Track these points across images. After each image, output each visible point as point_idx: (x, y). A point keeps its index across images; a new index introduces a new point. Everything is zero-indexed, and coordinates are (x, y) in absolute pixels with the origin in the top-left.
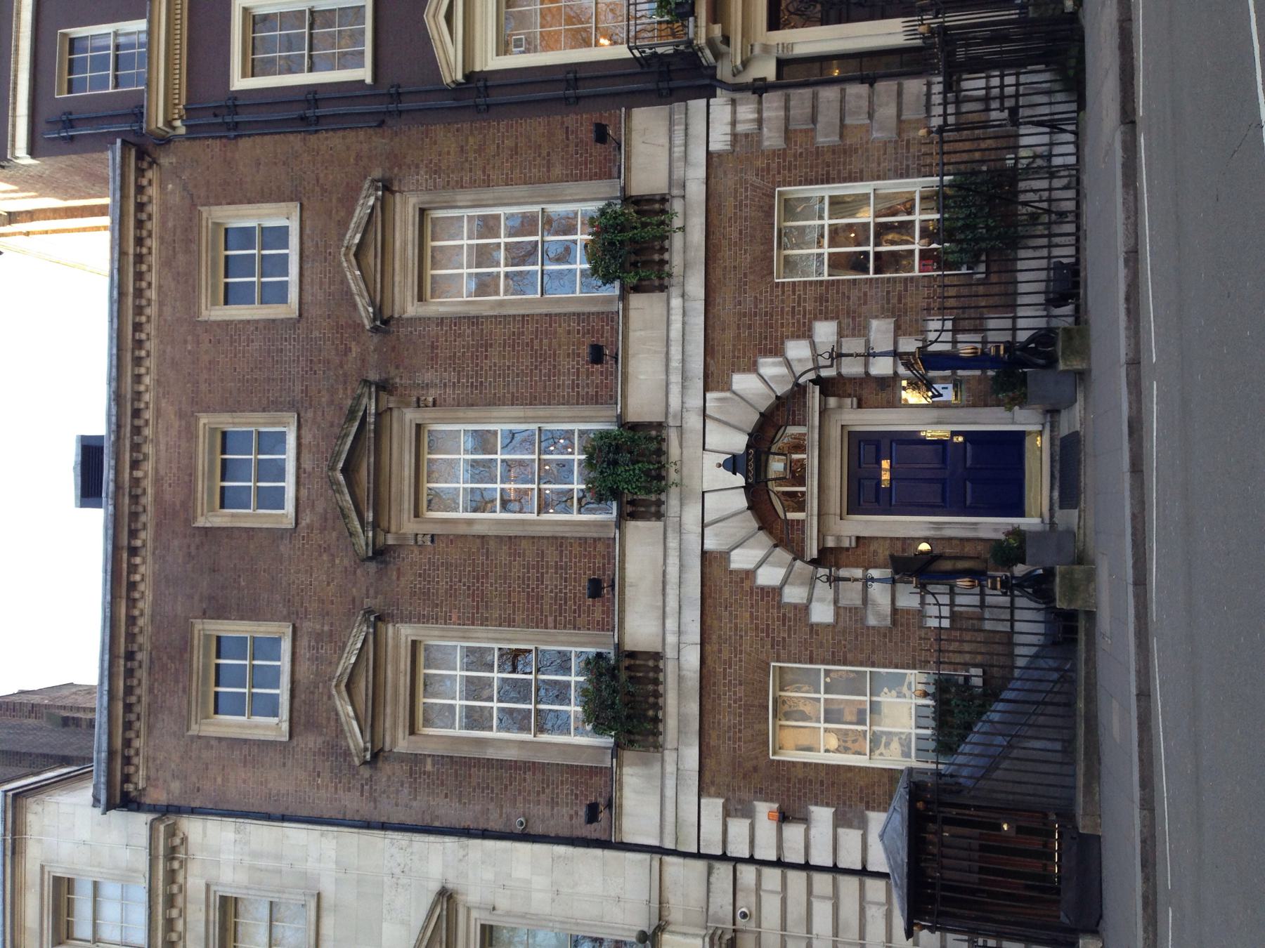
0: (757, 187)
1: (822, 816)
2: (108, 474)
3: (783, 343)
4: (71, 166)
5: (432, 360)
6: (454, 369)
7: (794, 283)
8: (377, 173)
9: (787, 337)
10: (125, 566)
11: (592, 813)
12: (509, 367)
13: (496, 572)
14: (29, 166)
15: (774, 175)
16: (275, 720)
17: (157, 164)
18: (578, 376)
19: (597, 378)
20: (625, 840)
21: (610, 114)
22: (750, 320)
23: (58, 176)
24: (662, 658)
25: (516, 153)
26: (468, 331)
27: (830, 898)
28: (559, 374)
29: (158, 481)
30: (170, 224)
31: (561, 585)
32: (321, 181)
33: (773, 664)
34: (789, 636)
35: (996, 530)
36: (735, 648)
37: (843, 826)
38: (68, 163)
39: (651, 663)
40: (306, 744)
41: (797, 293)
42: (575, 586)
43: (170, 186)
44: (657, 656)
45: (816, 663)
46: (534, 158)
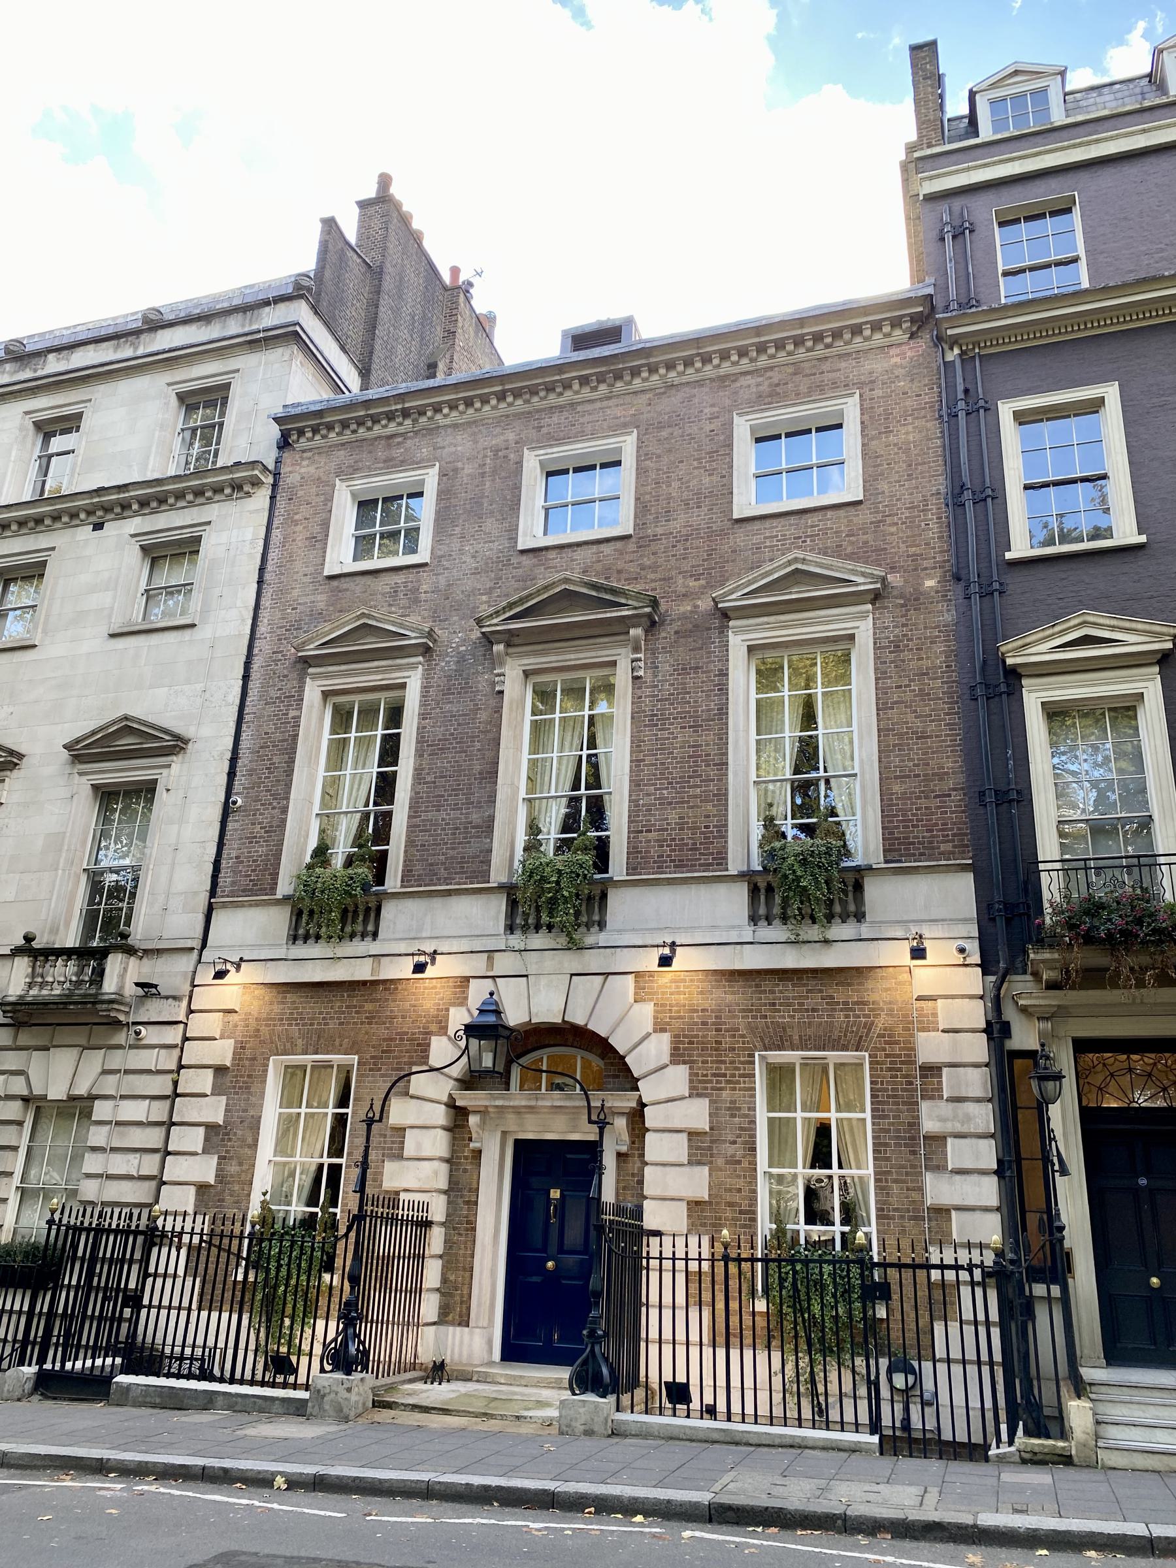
0: (870, 1029)
1: (932, 1117)
3: (684, 1063)
7: (754, 1076)
8: (895, 579)
9: (690, 1068)
10: (486, 391)
16: (753, 502)
19: (656, 852)
21: (967, 846)
24: (859, 921)
46: (913, 760)
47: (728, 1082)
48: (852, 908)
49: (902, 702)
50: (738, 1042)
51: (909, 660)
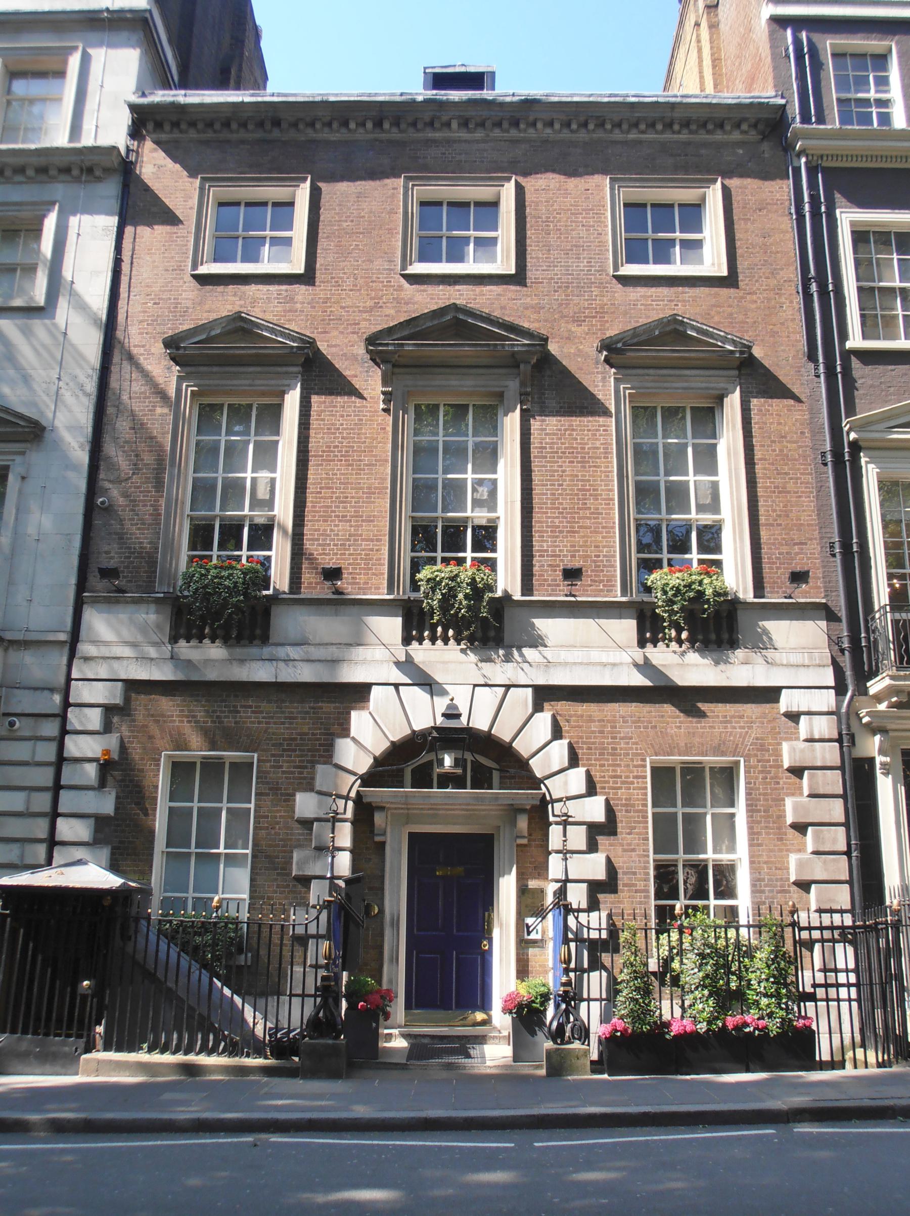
0: (744, 739)
2: (455, 95)
4: (760, 59)
5: (569, 408)
6: (560, 430)
11: (108, 573)
12: (562, 485)
13: (352, 474)
14: (759, 18)
15: (756, 755)
17: (762, 139)
18: (552, 556)
20: (85, 606)
22: (609, 732)
23: (751, 47)
25: (780, 492)
26: (598, 444)
27: (28, 809)
28: (553, 537)
29: (449, 142)
30: (703, 151)
31: (338, 540)
32: (748, 297)
33: (256, 755)
34: (283, 772)
35: (390, 981)
36: (272, 718)
37: (96, 823)
38: (763, 55)
39: (258, 632)
40: (185, 291)
41: (635, 781)
42: (336, 554)
43: (741, 152)
44: (265, 639)
45: (256, 800)
47: (623, 783)
48: (726, 636)
49: (765, 460)
50: (632, 749)
51: (771, 423)
